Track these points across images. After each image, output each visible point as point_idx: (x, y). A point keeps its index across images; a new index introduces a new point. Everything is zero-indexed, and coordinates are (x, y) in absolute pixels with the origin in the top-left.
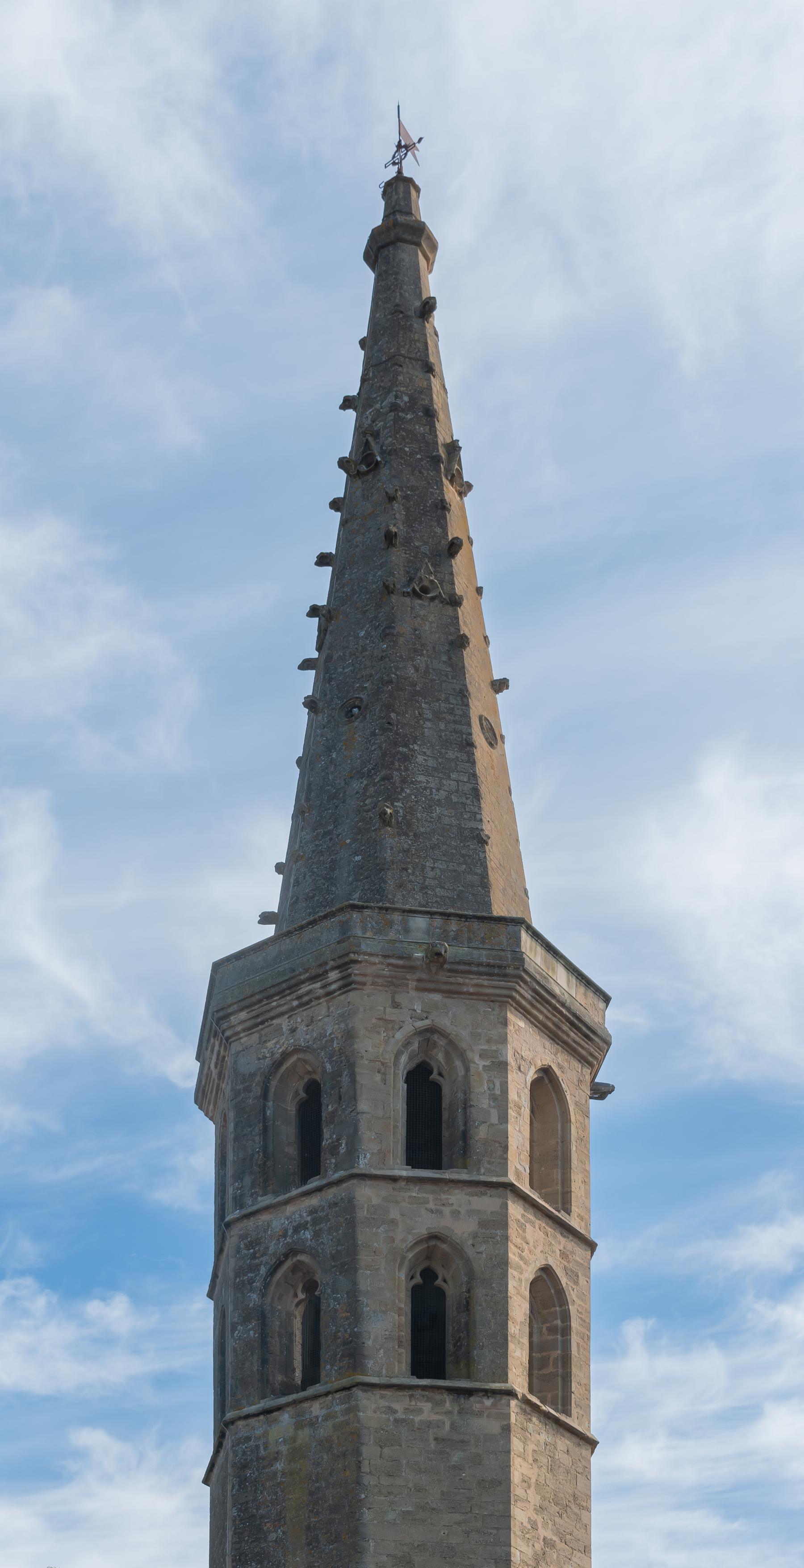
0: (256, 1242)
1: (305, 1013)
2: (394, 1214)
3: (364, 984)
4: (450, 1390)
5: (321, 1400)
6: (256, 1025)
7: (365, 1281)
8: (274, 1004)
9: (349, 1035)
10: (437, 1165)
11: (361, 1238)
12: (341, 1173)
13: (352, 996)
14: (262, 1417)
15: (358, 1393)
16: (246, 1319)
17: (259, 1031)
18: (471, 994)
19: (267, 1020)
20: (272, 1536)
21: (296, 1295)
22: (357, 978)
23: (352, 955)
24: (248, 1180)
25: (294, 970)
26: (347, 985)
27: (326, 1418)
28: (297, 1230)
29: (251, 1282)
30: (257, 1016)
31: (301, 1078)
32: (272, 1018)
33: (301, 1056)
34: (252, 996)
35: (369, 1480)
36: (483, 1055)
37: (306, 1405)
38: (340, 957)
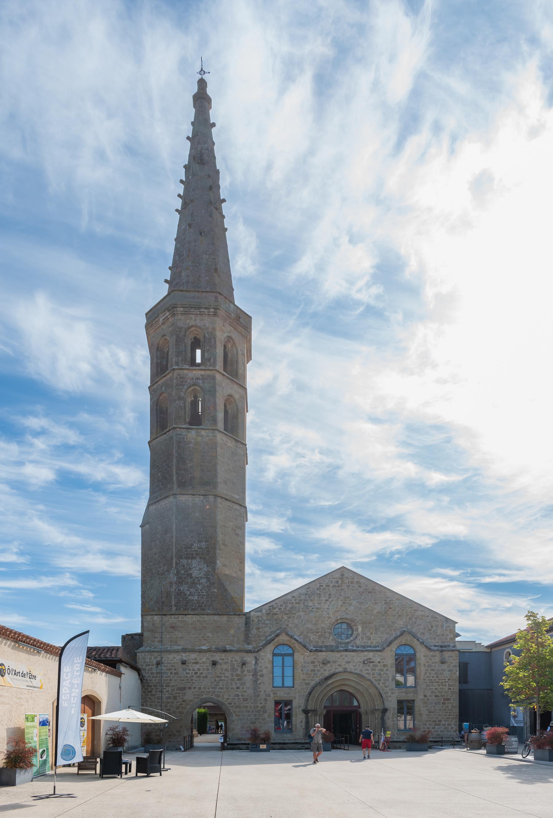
1: (200, 317)
3: (219, 316)
4: (235, 439)
5: (205, 431)
6: (185, 314)
7: (217, 399)
8: (192, 310)
9: (214, 329)
13: (216, 318)
14: (185, 430)
15: (216, 432)
17: (185, 316)
18: (239, 331)
19: (188, 314)
20: (189, 465)
21: (191, 398)
22: (219, 314)
23: (219, 307)
24: (180, 358)
25: (201, 303)
26: (215, 314)
27: (207, 436)
30: (186, 311)
31: (193, 335)
32: (190, 314)
33: (196, 328)
34: (185, 305)
35: (219, 458)
37: (200, 430)
38: (215, 306)
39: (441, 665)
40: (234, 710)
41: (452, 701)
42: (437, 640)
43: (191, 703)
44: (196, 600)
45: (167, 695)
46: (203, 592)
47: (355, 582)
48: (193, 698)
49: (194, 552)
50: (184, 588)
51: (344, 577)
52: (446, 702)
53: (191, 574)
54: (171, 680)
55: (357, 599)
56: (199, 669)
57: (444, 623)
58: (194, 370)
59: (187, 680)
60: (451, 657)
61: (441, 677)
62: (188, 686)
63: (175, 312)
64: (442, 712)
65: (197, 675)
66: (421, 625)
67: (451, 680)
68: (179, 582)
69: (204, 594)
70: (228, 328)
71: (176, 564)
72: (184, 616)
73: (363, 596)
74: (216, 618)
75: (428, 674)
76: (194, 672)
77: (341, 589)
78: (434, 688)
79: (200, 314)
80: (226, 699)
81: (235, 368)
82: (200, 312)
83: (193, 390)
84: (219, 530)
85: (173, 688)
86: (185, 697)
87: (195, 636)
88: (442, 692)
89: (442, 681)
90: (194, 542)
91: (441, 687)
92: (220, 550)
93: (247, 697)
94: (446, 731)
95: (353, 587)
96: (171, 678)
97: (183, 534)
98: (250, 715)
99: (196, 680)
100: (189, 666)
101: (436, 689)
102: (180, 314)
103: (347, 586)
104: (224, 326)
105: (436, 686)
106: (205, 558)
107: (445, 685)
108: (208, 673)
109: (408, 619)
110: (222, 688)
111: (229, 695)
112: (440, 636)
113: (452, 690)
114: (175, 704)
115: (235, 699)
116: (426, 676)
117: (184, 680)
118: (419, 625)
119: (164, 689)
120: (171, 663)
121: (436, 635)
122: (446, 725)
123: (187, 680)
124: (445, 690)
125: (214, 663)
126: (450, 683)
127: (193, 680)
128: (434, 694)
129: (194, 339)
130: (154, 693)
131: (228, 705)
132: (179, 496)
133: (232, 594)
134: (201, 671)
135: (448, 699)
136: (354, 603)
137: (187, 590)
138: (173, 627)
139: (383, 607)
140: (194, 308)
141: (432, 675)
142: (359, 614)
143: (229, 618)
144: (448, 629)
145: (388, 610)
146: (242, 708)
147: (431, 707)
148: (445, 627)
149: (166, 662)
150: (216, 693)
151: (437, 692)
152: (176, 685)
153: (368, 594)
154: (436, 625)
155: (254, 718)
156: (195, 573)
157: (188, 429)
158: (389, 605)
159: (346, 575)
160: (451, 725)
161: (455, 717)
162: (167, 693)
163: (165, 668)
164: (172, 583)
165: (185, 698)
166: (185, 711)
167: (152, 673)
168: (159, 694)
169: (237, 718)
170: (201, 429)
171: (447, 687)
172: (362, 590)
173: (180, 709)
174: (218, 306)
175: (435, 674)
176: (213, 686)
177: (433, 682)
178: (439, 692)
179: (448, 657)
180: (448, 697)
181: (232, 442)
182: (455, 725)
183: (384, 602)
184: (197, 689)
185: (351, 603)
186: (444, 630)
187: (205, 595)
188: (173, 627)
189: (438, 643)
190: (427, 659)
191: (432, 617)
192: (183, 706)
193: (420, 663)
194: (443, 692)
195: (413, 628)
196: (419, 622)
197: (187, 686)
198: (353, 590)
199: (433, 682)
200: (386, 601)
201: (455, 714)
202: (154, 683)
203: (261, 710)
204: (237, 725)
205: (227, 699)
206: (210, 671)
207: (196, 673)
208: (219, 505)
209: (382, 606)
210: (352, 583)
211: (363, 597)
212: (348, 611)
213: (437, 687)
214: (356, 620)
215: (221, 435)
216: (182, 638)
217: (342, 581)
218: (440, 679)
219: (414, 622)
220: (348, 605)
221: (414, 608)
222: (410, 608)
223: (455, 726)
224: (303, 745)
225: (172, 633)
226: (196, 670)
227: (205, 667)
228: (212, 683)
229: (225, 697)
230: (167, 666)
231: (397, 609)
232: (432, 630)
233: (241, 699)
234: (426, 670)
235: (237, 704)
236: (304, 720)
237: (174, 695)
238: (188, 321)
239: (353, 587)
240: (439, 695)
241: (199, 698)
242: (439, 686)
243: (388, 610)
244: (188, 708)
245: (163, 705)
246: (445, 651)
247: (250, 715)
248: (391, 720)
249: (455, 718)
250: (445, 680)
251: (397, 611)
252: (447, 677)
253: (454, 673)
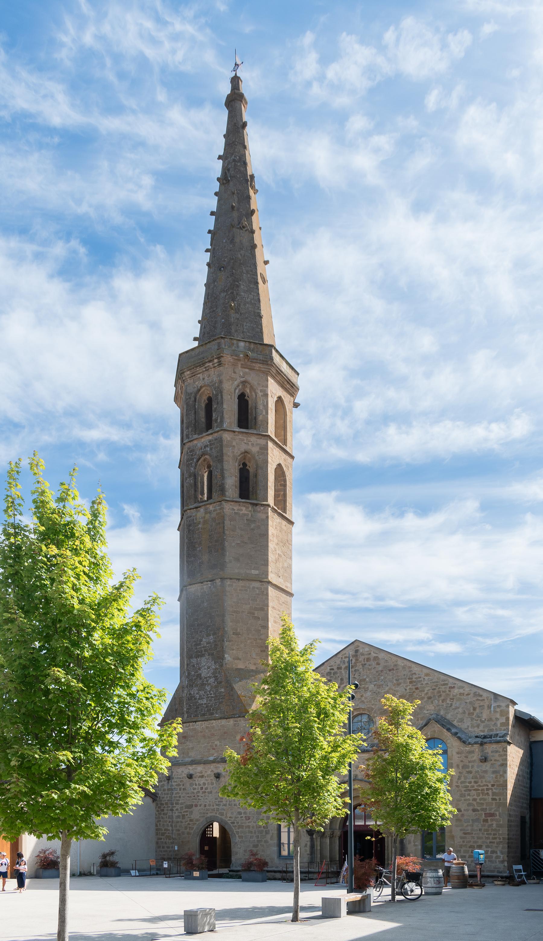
5: (213, 504)
6: (192, 376)
7: (226, 467)
9: (221, 382)
26: (220, 364)
27: (214, 511)
29: (191, 464)
30: (193, 373)
32: (197, 374)
36: (261, 391)
37: (208, 506)
39: (481, 764)
40: (237, 830)
41: (498, 817)
42: (481, 728)
43: (197, 823)
44: (205, 704)
45: (177, 814)
46: (211, 694)
47: (372, 659)
48: (200, 817)
49: (203, 649)
50: (194, 691)
51: (358, 654)
52: (489, 818)
53: (200, 674)
54: (180, 797)
55: (374, 682)
56: (204, 784)
57: (492, 702)
58: (202, 438)
59: (194, 796)
60: (497, 752)
61: (482, 782)
62: (195, 803)
63: (184, 379)
64: (483, 833)
65: (203, 790)
66: (459, 708)
67: (495, 787)
68: (190, 685)
69: (212, 695)
70: (241, 371)
71: (188, 665)
72: (194, 723)
73: (382, 675)
74: (224, 722)
75: (463, 779)
76: (200, 787)
77: (355, 670)
78: (471, 798)
79: (206, 370)
80: (230, 818)
81: (254, 416)
82: (205, 368)
83: (204, 460)
84: (228, 619)
85: (182, 806)
86: (192, 816)
87: (204, 745)
88: (482, 804)
89: (483, 788)
90: (203, 637)
91: (481, 796)
92: (229, 641)
93: (249, 814)
94: (489, 861)
95: (370, 665)
96: (180, 795)
97: (193, 629)
98: (253, 836)
99: (202, 797)
100: (195, 781)
101: (475, 800)
102: (189, 378)
103: (362, 664)
104: (235, 373)
105: (474, 795)
106: (212, 654)
107: (488, 793)
108: (213, 787)
109: (441, 701)
110: (225, 805)
111: (232, 813)
112: (486, 722)
113: (498, 801)
114: (184, 823)
115: (238, 817)
116: (460, 781)
117: (191, 797)
118: (456, 709)
119: (174, 807)
120: (180, 778)
121: (481, 721)
122: (489, 852)
123: (194, 796)
124: (487, 801)
125: (218, 776)
126: (494, 791)
127: (199, 796)
128: (471, 808)
129: (208, 400)
130: (166, 812)
131: (231, 825)
132: (190, 587)
133: (239, 693)
134: (206, 786)
135: (492, 815)
136: (371, 687)
137: (197, 693)
139: (408, 688)
140: (199, 366)
141: (468, 780)
142: (377, 702)
143: (235, 721)
144: (498, 710)
145: (414, 692)
146: (244, 828)
147: (467, 826)
148: (494, 707)
149: (176, 776)
150: (220, 811)
151: (476, 805)
152: (185, 803)
153: (388, 672)
154: (480, 706)
155: (256, 840)
156: (204, 673)
157: (196, 508)
158: (415, 684)
159: (361, 651)
160: (496, 853)
161: (501, 840)
162: (177, 812)
163: (175, 783)
164: (184, 688)
165: (192, 817)
166: (192, 831)
167: (164, 790)
168: (170, 813)
169: (240, 840)
170: (208, 504)
171: (491, 797)
172: (380, 669)
173: (188, 829)
174: (220, 354)
175: (472, 778)
176: (217, 803)
177: (470, 790)
178: (478, 803)
179: (492, 752)
180: (492, 812)
181: (247, 508)
182: (502, 853)
183: (408, 681)
184: (202, 807)
185: (368, 688)
186: (492, 712)
187: (213, 697)
189: (483, 731)
190: (461, 757)
191: (475, 694)
192: (190, 826)
193: (452, 763)
194: (485, 804)
195: (448, 713)
196: (456, 703)
197: (194, 804)
198: (369, 670)
199: (470, 790)
200: (412, 679)
201: (501, 837)
202: (166, 800)
203: (263, 830)
204: (240, 848)
205: (230, 817)
206: (215, 785)
207: (202, 788)
208: (228, 589)
209: (407, 686)
210: (368, 660)
211: (382, 678)
212: (363, 699)
213: (475, 797)
214: (372, 709)
215: (231, 505)
216: (193, 748)
217: (357, 660)
218: (480, 786)
219: (449, 705)
220: (363, 690)
221: (450, 685)
222: (444, 685)
223: (502, 854)
224: (306, 875)
225: (184, 743)
226: (202, 784)
227: (210, 781)
228: (216, 799)
229: (229, 815)
230: (176, 782)
231: (427, 689)
232: (475, 714)
233: (244, 817)
234: (460, 772)
235: (240, 824)
236: (309, 844)
237: (183, 814)
238: (197, 383)
239: (370, 665)
240: (479, 808)
241: (204, 816)
242: (478, 795)
243: (414, 692)
244: (195, 828)
245: (173, 825)
246: (486, 743)
247: (253, 836)
248: (413, 844)
249: (501, 842)
250: (488, 786)
251: (426, 692)
252: (490, 782)
253: (500, 775)
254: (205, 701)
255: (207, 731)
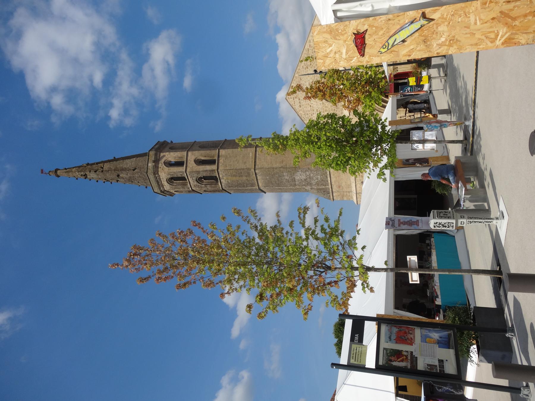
0: (195, 186)
2: (191, 166)
10: (183, 162)
11: (195, 171)
12: (185, 173)
16: (207, 187)
20: (240, 182)
28: (193, 180)
138: (339, 187)
156: (303, 177)
187: (317, 172)
188: (339, 187)
254: (319, 177)
255: (335, 175)
